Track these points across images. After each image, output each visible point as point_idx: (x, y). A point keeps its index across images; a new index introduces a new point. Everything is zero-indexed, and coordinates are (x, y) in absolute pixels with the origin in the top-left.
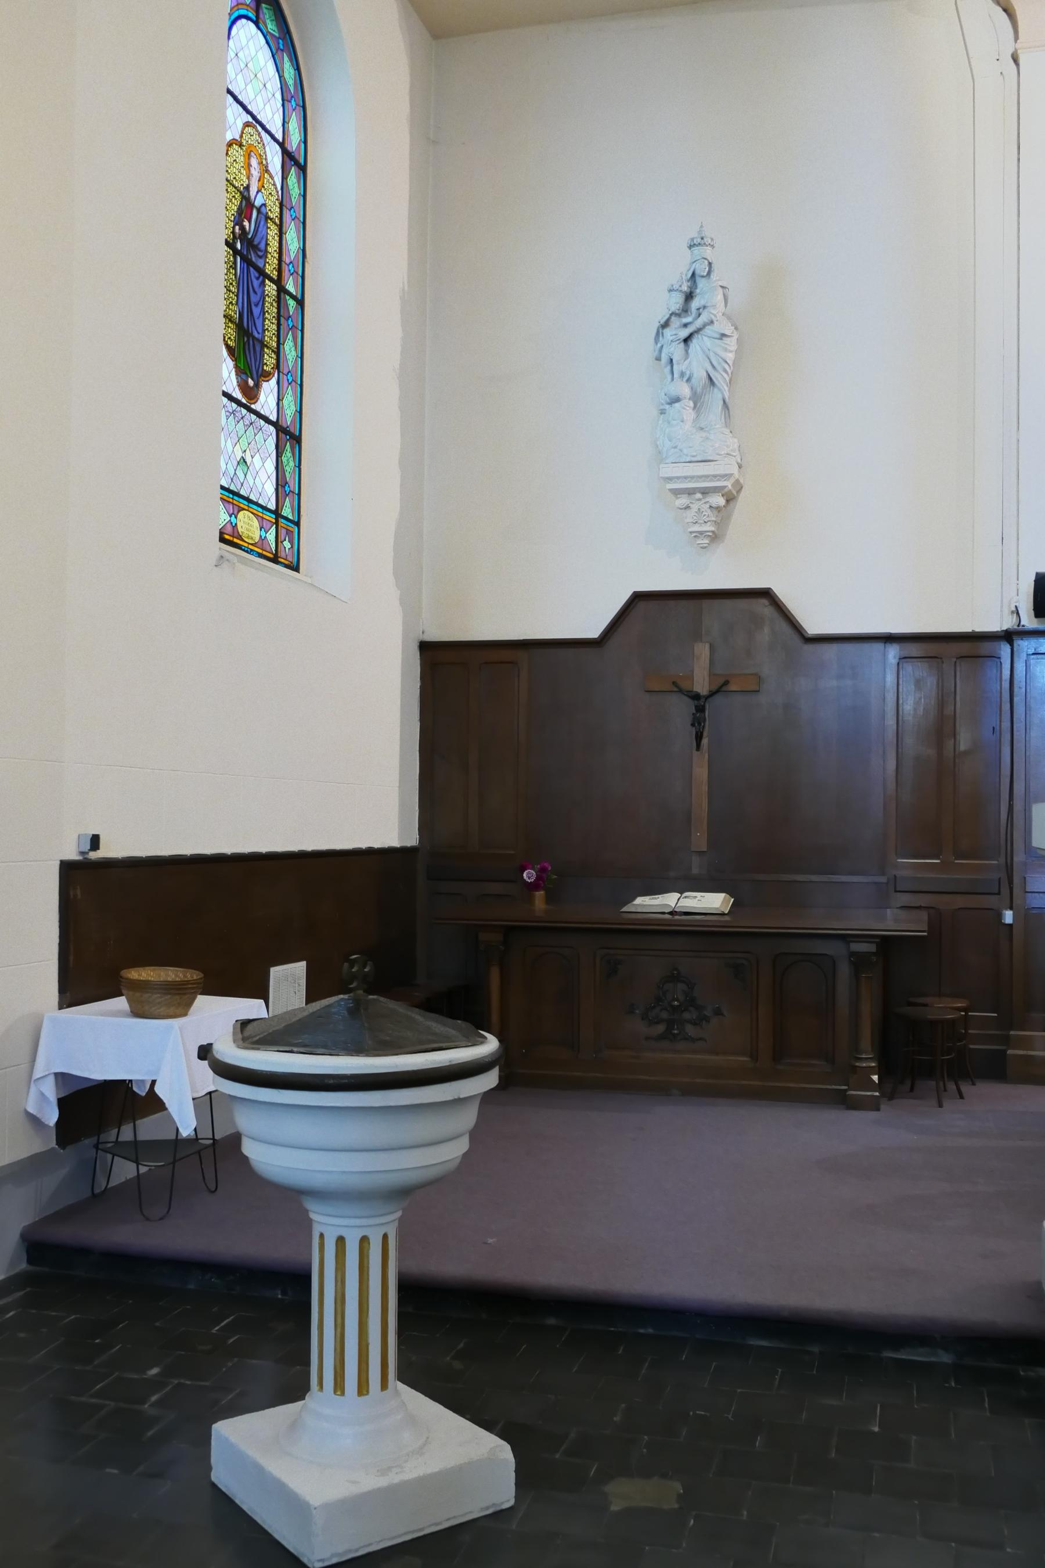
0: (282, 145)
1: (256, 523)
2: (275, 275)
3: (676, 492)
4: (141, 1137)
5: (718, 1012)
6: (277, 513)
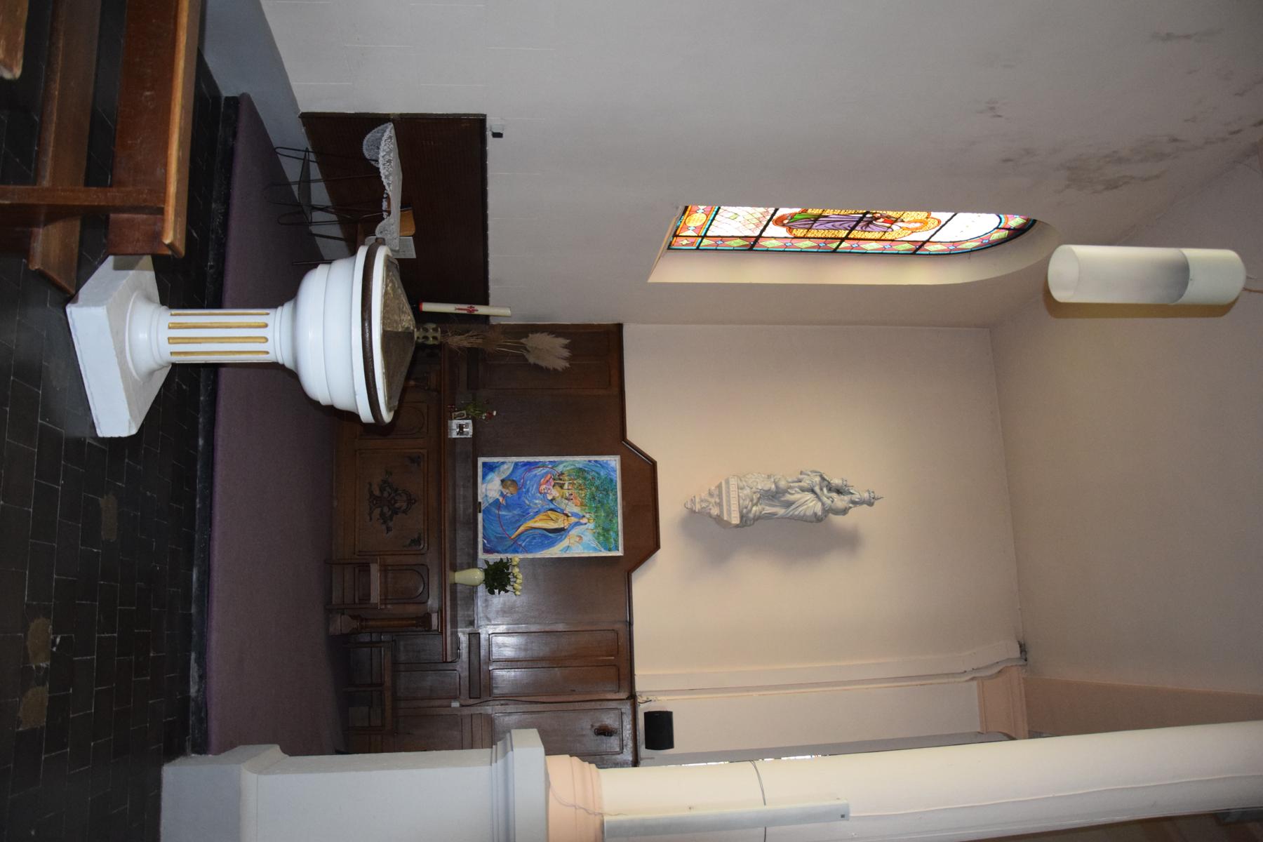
0: (928, 241)
1: (699, 224)
2: (851, 236)
3: (719, 487)
4: (313, 185)
5: (389, 529)
6: (705, 236)
